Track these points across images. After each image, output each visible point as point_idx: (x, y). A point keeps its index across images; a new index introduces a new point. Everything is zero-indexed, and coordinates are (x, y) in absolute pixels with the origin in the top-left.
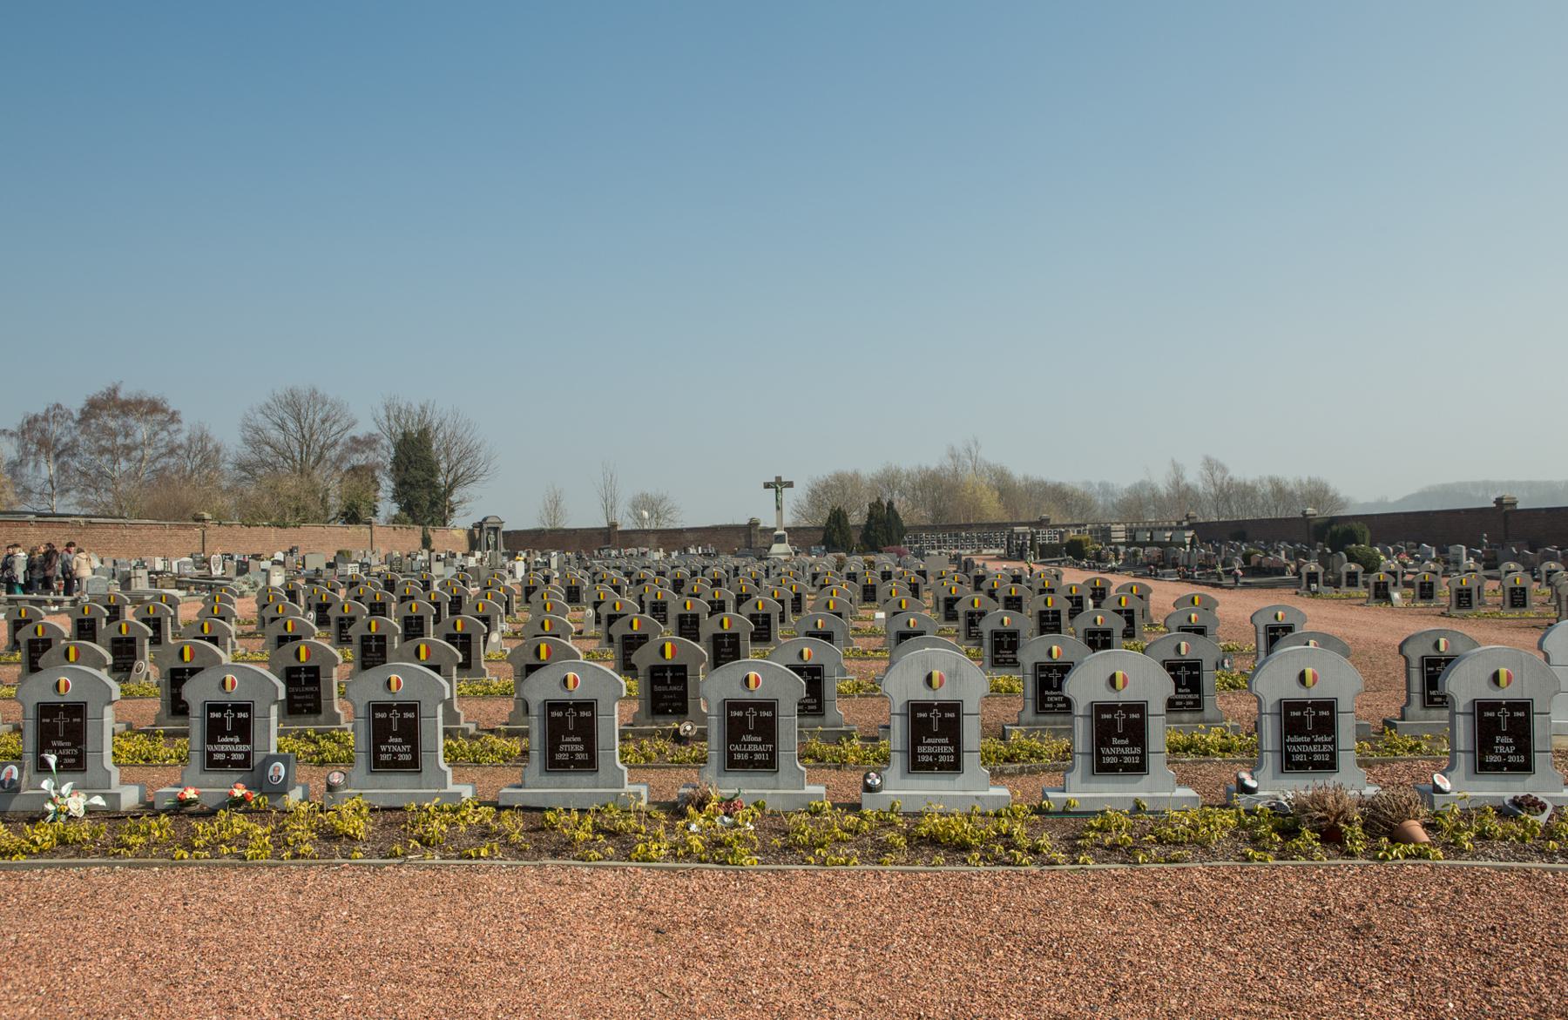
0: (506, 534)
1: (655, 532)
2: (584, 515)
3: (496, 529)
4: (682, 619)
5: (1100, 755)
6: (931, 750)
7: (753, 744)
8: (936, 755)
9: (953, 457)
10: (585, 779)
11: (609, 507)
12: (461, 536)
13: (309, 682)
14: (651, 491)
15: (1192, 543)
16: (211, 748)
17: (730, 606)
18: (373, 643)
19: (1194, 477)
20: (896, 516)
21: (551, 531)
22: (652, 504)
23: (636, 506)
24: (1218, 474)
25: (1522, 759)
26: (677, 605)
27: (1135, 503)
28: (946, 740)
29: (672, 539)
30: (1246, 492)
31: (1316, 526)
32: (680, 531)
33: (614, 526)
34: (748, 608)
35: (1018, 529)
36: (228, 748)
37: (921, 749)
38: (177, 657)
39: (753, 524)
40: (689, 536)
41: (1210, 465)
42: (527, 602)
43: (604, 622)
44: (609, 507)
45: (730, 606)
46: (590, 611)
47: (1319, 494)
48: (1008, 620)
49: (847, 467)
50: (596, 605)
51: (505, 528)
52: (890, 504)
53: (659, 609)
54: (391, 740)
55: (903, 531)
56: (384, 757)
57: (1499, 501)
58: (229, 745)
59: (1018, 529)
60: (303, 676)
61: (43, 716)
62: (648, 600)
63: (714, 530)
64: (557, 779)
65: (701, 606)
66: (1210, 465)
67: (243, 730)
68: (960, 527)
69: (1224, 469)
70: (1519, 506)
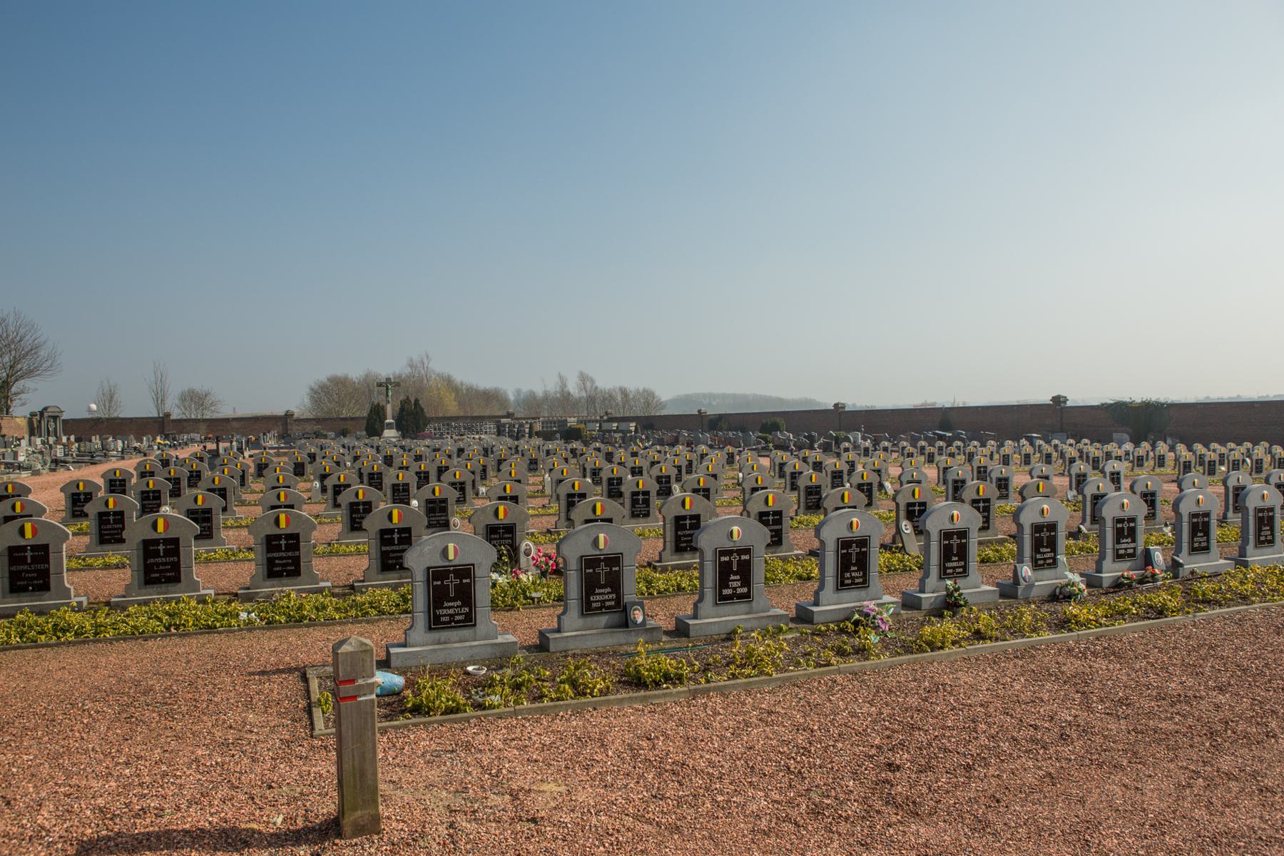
0: (65, 422)
1: (205, 420)
2: (137, 405)
3: (55, 418)
4: (395, 488)
5: (721, 592)
6: (598, 598)
7: (451, 608)
8: (603, 601)
9: (411, 366)
10: (1270, 550)
11: (160, 399)
12: (23, 423)
13: (404, 490)
14: (199, 386)
15: (636, 431)
16: (1118, 547)
17: (433, 476)
18: (641, 497)
19: (573, 388)
20: (422, 410)
21: (107, 419)
22: (194, 398)
23: (183, 398)
24: (588, 385)
25: (745, 590)
26: (392, 477)
27: (532, 402)
28: (609, 590)
29: (219, 428)
30: (608, 398)
31: (711, 421)
32: (227, 420)
33: (168, 415)
34: (447, 477)
35: (503, 420)
36: (451, 611)
37: (949, 565)
38: (762, 503)
39: (288, 415)
40: (235, 424)
41: (584, 378)
42: (499, 470)
43: (330, 491)
44: (160, 399)
45: (433, 476)
46: (317, 484)
47: (648, 396)
48: (815, 478)
49: (339, 372)
50: (323, 477)
51: (65, 416)
52: (417, 401)
53: (375, 480)
54: (732, 577)
55: (428, 421)
56: (1196, 545)
57: (836, 405)
58: (1126, 544)
59: (503, 420)
60: (688, 522)
61: (434, 579)
62: (589, 467)
63: (256, 419)
64: (728, 608)
65: (408, 477)
66: (584, 378)
67: (1132, 533)
68: (451, 419)
69: (592, 381)
70: (1069, 404)
